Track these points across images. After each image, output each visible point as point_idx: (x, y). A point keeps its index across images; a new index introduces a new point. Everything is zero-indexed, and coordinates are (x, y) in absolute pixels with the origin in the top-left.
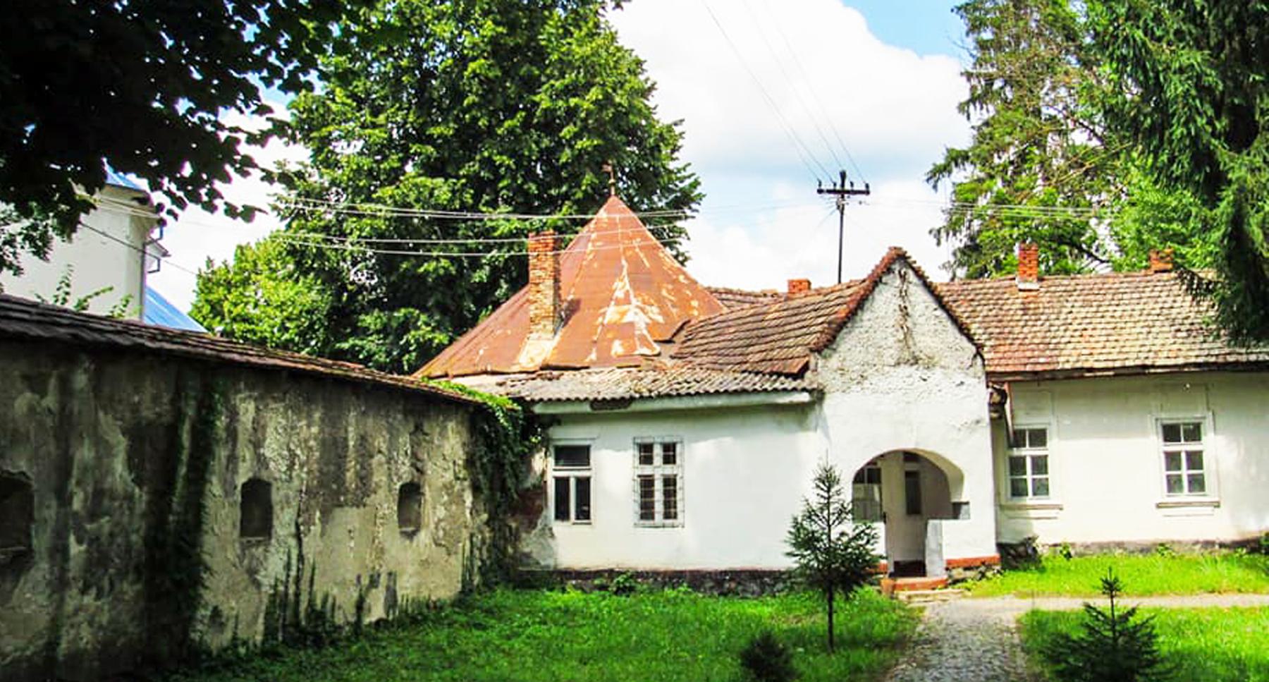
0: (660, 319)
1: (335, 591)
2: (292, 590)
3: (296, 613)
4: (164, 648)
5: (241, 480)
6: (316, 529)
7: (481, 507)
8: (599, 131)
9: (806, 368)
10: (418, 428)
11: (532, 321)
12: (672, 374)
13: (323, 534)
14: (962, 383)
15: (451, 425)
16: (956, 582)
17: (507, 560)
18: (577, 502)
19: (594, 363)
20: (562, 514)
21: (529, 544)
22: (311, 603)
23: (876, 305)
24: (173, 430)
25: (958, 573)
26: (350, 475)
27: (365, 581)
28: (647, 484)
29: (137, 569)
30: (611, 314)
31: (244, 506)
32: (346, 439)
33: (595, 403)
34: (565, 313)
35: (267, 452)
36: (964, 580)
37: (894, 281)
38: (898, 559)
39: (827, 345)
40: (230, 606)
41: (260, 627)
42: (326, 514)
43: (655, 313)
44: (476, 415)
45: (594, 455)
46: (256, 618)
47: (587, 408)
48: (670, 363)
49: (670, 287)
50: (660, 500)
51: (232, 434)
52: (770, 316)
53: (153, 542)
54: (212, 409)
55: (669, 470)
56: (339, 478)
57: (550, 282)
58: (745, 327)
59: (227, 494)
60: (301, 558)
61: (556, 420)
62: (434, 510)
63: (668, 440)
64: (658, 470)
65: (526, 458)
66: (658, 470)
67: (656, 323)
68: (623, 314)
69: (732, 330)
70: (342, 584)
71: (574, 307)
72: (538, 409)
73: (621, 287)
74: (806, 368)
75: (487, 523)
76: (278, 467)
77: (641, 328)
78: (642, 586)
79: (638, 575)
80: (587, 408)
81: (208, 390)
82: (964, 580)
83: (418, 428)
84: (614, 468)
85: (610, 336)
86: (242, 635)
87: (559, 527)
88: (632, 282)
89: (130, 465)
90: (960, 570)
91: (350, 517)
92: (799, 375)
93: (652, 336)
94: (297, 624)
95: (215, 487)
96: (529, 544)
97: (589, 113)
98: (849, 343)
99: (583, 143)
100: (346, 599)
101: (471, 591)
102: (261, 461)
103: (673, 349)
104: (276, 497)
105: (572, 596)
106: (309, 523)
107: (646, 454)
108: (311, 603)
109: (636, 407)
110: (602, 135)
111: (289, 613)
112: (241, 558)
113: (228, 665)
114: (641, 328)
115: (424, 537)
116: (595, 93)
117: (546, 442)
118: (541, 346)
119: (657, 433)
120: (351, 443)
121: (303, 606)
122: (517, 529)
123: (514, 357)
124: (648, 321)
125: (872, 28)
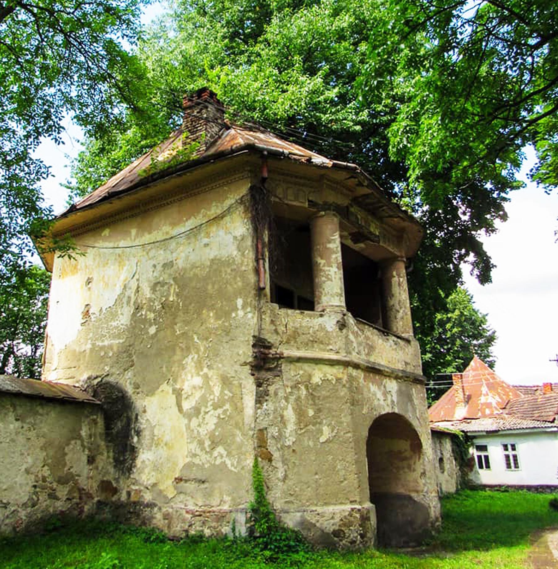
0: (500, 400)
8: (460, 325)
9: (554, 419)
10: (440, 442)
12: (510, 422)
15: (447, 440)
18: (486, 463)
20: (481, 467)
21: (471, 476)
28: (507, 457)
30: (483, 399)
33: (487, 432)
34: (468, 399)
43: (497, 398)
44: (453, 437)
47: (485, 434)
48: (506, 416)
50: (512, 462)
55: (514, 453)
57: (461, 390)
61: (475, 437)
62: (447, 466)
63: (513, 443)
64: (510, 453)
66: (510, 453)
68: (487, 399)
72: (469, 434)
73: (484, 389)
74: (554, 419)
77: (494, 404)
78: (510, 489)
79: (508, 486)
80: (485, 434)
83: (440, 442)
84: (495, 452)
85: (484, 407)
87: (480, 471)
88: (488, 387)
92: (553, 422)
96: (471, 476)
97: (456, 319)
99: (455, 330)
103: (506, 411)
105: (488, 492)
107: (506, 447)
109: (500, 433)
110: (462, 326)
114: (494, 404)
115: (446, 473)
116: (457, 312)
117: (473, 444)
118: (461, 412)
119: (509, 441)
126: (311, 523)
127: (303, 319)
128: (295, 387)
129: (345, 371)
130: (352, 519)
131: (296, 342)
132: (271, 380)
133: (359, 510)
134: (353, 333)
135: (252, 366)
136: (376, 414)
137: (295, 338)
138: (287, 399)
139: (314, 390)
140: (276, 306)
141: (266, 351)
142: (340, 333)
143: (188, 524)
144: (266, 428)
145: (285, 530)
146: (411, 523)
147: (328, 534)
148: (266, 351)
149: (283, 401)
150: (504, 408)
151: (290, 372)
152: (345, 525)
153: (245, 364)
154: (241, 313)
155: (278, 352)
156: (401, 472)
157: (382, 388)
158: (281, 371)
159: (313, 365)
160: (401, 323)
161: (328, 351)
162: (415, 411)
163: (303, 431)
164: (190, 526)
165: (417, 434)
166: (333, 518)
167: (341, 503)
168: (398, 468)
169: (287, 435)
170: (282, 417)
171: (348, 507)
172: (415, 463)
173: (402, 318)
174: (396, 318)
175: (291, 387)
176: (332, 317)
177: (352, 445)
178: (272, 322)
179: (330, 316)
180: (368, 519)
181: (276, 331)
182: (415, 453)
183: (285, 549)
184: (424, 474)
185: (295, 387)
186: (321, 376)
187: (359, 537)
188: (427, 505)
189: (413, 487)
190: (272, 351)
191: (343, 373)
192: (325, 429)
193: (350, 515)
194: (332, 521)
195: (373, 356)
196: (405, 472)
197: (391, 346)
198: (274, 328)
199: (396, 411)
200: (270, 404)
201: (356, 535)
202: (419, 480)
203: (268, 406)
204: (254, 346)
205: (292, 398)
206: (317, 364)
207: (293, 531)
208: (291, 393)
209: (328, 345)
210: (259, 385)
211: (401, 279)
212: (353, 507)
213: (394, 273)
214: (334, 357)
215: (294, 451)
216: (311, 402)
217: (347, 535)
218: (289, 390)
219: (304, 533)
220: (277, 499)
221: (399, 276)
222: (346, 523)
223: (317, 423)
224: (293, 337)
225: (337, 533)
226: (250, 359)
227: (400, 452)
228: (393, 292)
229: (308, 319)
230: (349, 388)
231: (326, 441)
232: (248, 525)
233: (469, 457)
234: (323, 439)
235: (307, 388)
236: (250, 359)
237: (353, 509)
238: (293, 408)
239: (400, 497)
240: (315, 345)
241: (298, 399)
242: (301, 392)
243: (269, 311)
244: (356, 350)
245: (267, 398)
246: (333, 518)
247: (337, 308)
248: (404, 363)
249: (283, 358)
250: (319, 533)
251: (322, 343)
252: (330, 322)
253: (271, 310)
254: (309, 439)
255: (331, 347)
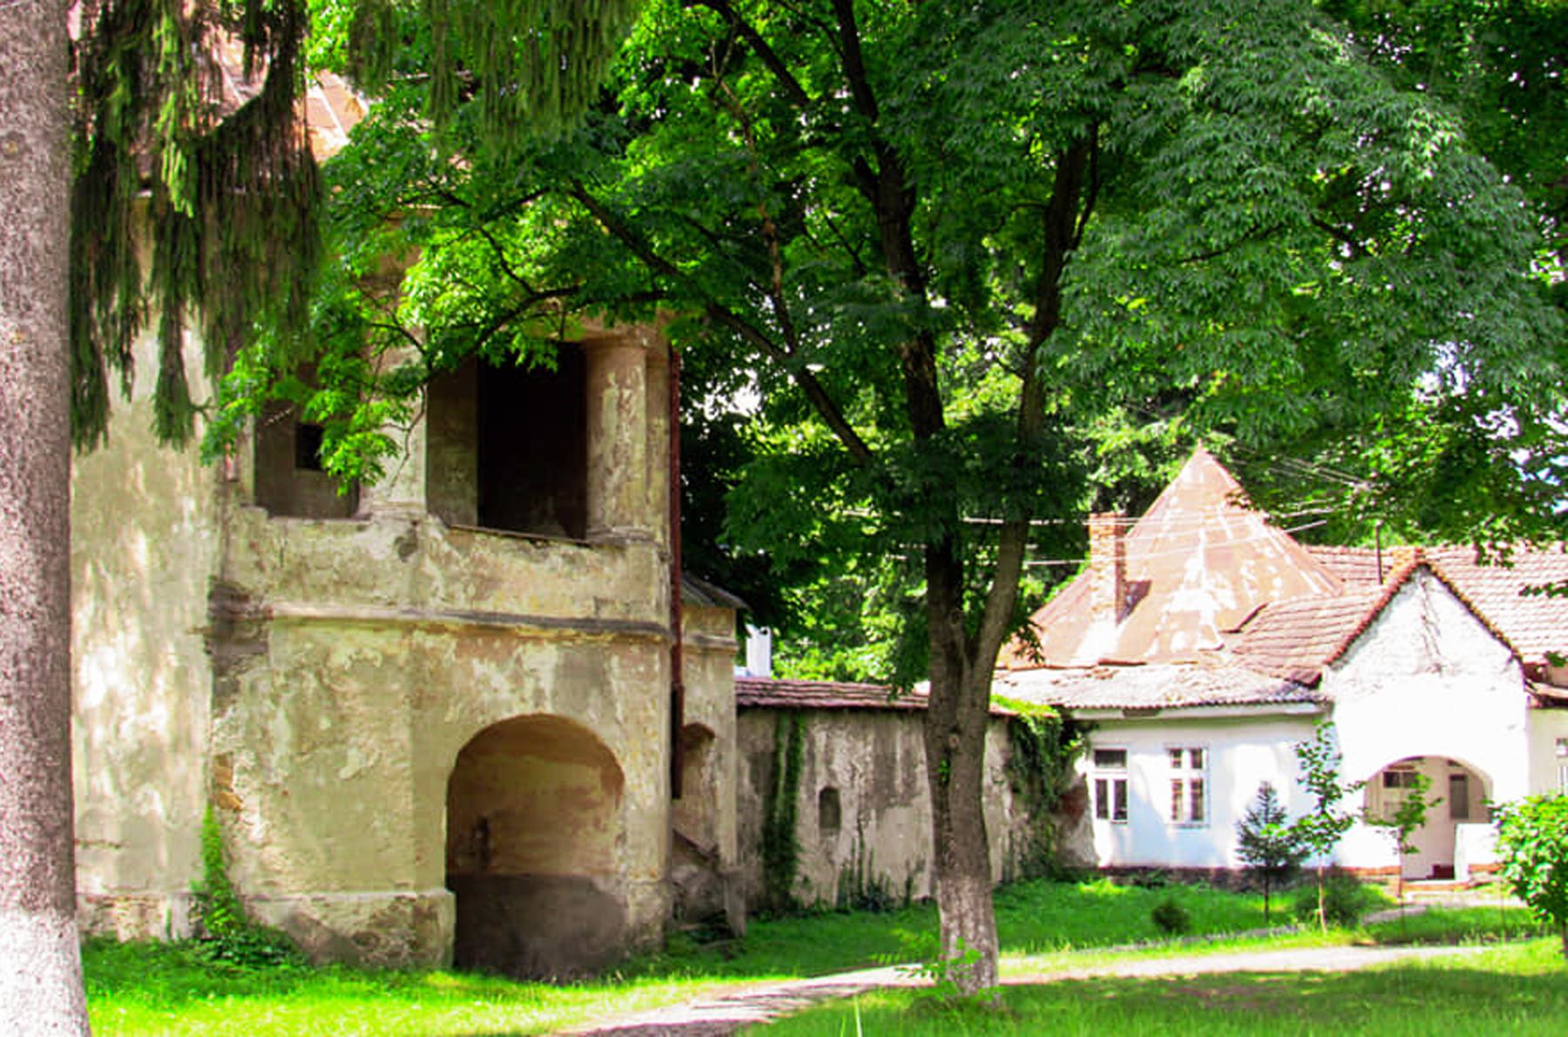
1: (888, 872)
2: (856, 868)
3: (860, 886)
4: (775, 897)
5: (819, 788)
6: (873, 823)
7: (1021, 807)
11: (1095, 609)
13: (878, 826)
14: (1493, 689)
16: (1479, 885)
17: (1051, 856)
19: (1152, 658)
20: (1102, 813)
22: (871, 880)
23: (1392, 616)
24: (775, 754)
25: (1481, 876)
26: (898, 782)
27: (913, 866)
28: (1177, 786)
29: (759, 848)
31: (822, 807)
32: (894, 754)
33: (1126, 710)
34: (1132, 595)
35: (835, 767)
36: (1487, 884)
37: (1415, 593)
38: (1438, 862)
39: (1340, 656)
40: (815, 876)
41: (835, 893)
42: (880, 813)
45: (1130, 758)
46: (831, 885)
47: (1120, 715)
49: (1252, 563)
51: (812, 756)
52: (1321, 613)
53: (767, 831)
54: (798, 740)
56: (889, 784)
58: (1302, 623)
59: (810, 798)
60: (862, 845)
61: (1094, 725)
63: (1195, 746)
65: (1066, 762)
67: (1226, 610)
69: (1288, 625)
70: (894, 867)
71: (1142, 589)
72: (1076, 715)
73: (1195, 565)
75: (1028, 822)
76: (843, 779)
77: (1207, 619)
80: (1120, 715)
81: (795, 725)
82: (1487, 884)
84: (1150, 772)
85: (1173, 626)
86: (823, 896)
89: (753, 781)
90: (1485, 874)
91: (899, 814)
93: (1219, 624)
94: (860, 893)
95: (802, 794)
98: (1363, 657)
100: (898, 878)
101: (1011, 881)
102: (832, 774)
103: (1237, 641)
104: (843, 800)
106: (868, 819)
108: (871, 880)
109: (1162, 715)
111: (855, 886)
112: (821, 842)
113: (815, 914)
114: (1207, 619)
119: (1186, 739)
120: (898, 757)
121: (865, 881)
122: (1062, 828)
123: (1073, 651)
124: (1218, 608)
125: (599, 1031)
126: (311, 920)
127: (318, 537)
128: (295, 674)
129: (406, 641)
130: (396, 915)
131: (302, 585)
132: (245, 662)
133: (412, 900)
134: (436, 558)
135: (206, 635)
136: (483, 721)
137: (299, 576)
138: (275, 699)
139: (334, 679)
140: (262, 512)
141: (237, 606)
142: (400, 564)
143: (90, 921)
144: (231, 753)
145: (260, 929)
146: (587, 936)
147: (344, 939)
148: (237, 606)
149: (268, 702)
150: (1237, 631)
151: (283, 648)
152: (380, 925)
153: (196, 630)
154: (188, 526)
155: (261, 607)
156: (581, 833)
157: (511, 665)
158: (265, 645)
159: (334, 631)
160: (614, 500)
161: (372, 601)
162: (612, 704)
163: (307, 757)
164: (95, 923)
165: (612, 758)
166: (356, 912)
167: (376, 888)
168: (577, 825)
169: (273, 765)
170: (265, 732)
171: (391, 894)
172: (608, 815)
173: (618, 489)
174: (604, 488)
175: (287, 676)
176: (386, 531)
177: (409, 783)
178: (252, 546)
179: (380, 528)
180: (432, 915)
181: (260, 566)
182: (610, 794)
183: (253, 958)
184: (622, 838)
185: (295, 674)
186: (351, 651)
187: (406, 947)
188: (621, 901)
189: (600, 864)
190: (250, 607)
191: (400, 644)
192: (353, 754)
193: (393, 908)
194: (353, 918)
195: (491, 600)
196: (587, 833)
197: (553, 569)
198: (255, 558)
199: (548, 709)
200: (241, 706)
201: (401, 942)
202: (612, 850)
203: (238, 711)
204: (211, 597)
205: (286, 696)
206: (344, 628)
207: (276, 932)
208: (286, 687)
209: (373, 588)
210: (219, 671)
211: (627, 393)
212: (400, 894)
213: (611, 377)
214: (383, 613)
215: (285, 793)
216: (326, 703)
217: (383, 942)
218: (281, 680)
219: (298, 936)
220: (246, 877)
221: (621, 383)
222: (382, 922)
223: (335, 741)
224: (295, 575)
225: (361, 939)
226: (205, 623)
227: (581, 791)
228: (604, 425)
229: (331, 537)
230: (411, 674)
231: (354, 776)
232: (193, 920)
233: (1074, 782)
234: (346, 772)
235: (319, 675)
236: (205, 623)
237: (398, 899)
238: (288, 716)
239: (571, 882)
240: (344, 590)
241: (299, 698)
242: (305, 684)
243: (245, 526)
244: (441, 594)
245: (234, 697)
246: (356, 912)
247: (399, 510)
248: (592, 603)
249: (271, 619)
250: (325, 937)
251: (358, 585)
252: (378, 542)
253: (251, 523)
254: (317, 774)
255: (377, 593)
